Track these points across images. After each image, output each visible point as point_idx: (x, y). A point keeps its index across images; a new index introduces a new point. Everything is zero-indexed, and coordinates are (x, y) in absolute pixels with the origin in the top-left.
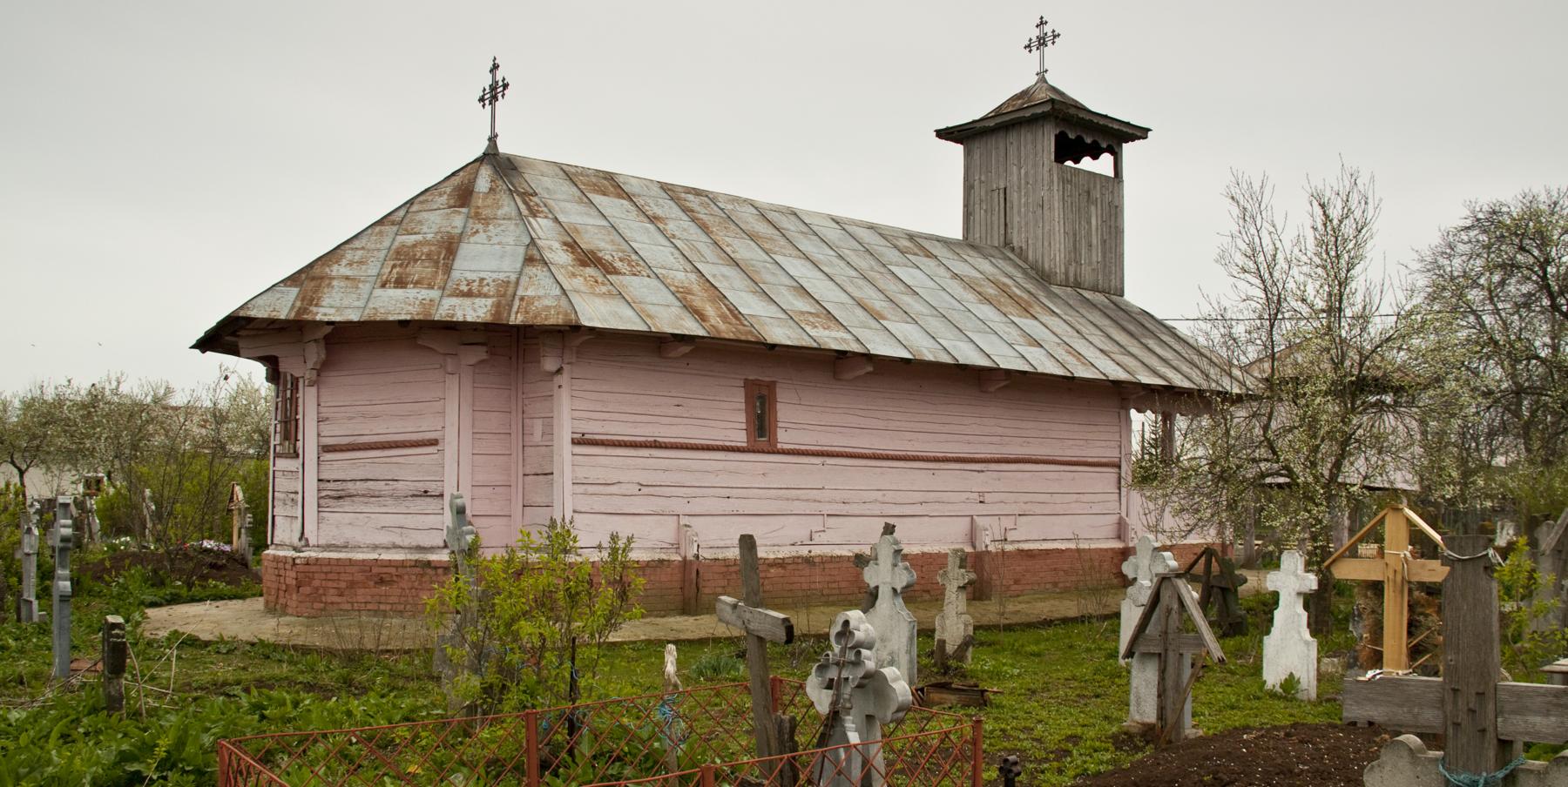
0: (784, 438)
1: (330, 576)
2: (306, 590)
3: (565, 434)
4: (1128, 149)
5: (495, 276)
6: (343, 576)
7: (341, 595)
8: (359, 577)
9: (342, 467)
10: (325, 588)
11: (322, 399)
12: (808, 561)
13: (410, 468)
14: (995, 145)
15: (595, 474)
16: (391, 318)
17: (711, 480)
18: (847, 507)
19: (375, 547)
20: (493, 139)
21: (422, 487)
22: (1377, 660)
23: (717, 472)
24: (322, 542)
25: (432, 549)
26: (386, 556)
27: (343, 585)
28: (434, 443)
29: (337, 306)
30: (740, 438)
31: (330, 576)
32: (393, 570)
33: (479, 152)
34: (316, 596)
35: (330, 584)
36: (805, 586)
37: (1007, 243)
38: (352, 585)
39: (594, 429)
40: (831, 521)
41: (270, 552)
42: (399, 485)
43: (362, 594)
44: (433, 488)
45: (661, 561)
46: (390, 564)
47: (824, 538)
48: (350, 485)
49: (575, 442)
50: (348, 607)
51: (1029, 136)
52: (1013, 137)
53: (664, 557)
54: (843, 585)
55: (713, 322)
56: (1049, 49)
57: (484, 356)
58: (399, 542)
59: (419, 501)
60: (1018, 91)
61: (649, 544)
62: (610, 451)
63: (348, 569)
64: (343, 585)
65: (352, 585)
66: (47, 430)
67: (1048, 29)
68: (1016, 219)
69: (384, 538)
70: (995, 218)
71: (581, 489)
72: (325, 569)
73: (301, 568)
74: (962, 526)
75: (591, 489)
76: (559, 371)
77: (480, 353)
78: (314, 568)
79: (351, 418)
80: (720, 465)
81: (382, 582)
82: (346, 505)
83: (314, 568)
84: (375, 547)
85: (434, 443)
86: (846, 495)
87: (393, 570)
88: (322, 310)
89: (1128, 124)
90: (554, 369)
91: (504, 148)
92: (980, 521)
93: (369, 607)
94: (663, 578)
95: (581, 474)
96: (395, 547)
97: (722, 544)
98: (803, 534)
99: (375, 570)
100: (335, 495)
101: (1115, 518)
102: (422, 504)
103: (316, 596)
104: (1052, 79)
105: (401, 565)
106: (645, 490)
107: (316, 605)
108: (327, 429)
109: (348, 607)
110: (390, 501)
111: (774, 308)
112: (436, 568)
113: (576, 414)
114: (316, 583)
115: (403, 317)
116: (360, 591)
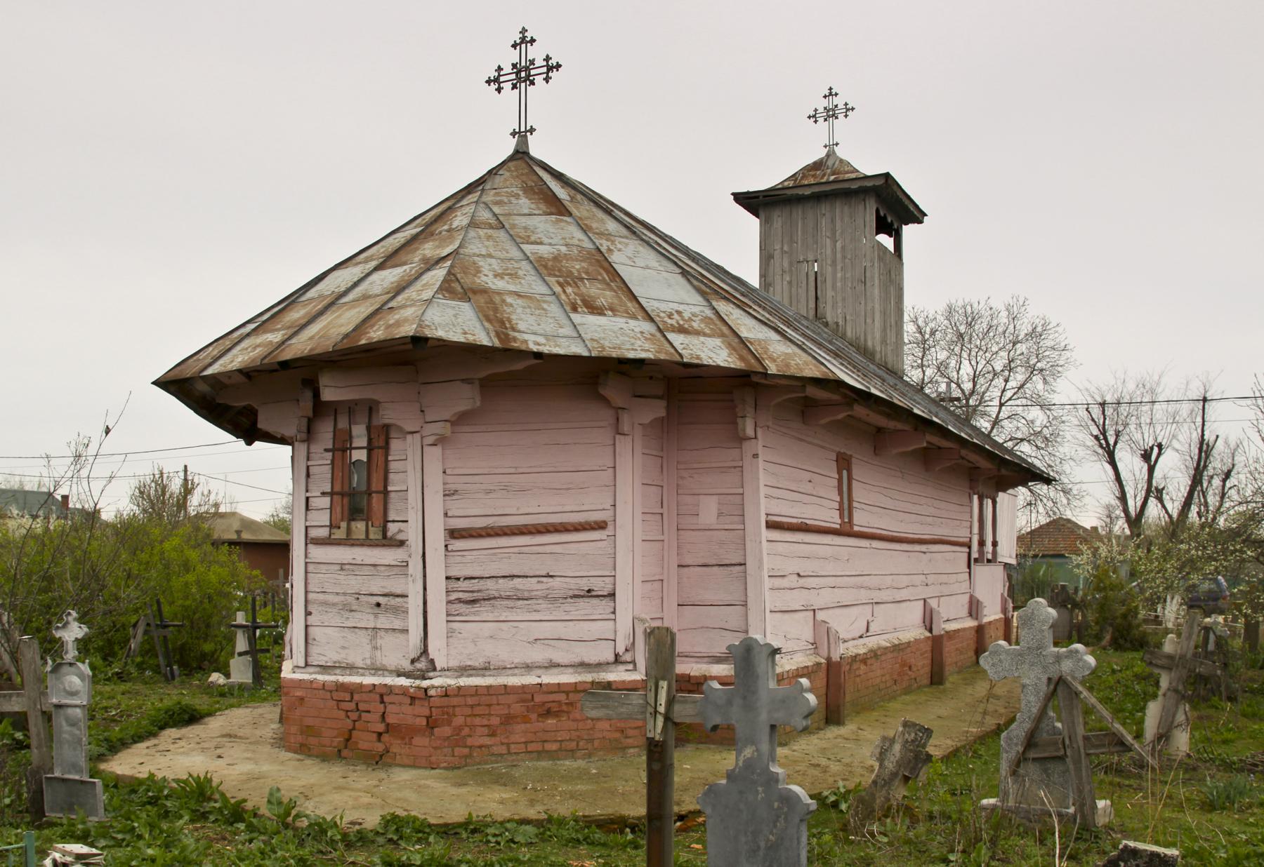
1: (478, 710)
2: (445, 731)
4: (908, 231)
6: (496, 710)
7: (493, 734)
8: (517, 709)
9: (479, 558)
10: (472, 727)
13: (572, 559)
14: (801, 217)
19: (528, 667)
20: (522, 135)
21: (585, 584)
25: (599, 666)
26: (550, 678)
27: (495, 721)
28: (601, 526)
31: (478, 710)
32: (562, 697)
33: (510, 151)
34: (457, 740)
35: (477, 721)
37: (818, 316)
38: (508, 720)
43: (519, 733)
46: (559, 688)
48: (490, 584)
49: (771, 525)
50: (503, 750)
51: (846, 209)
52: (825, 208)
56: (840, 122)
58: (559, 657)
59: (582, 603)
60: (810, 161)
63: (502, 699)
64: (495, 721)
65: (508, 720)
66: (20, 497)
67: (839, 101)
68: (830, 293)
69: (538, 655)
70: (802, 292)
72: (470, 701)
73: (436, 702)
74: (917, 611)
78: (455, 701)
79: (489, 492)
81: (548, 713)
82: (484, 612)
83: (455, 701)
84: (528, 667)
85: (601, 526)
87: (562, 697)
89: (601, 197)
91: (537, 149)
92: (933, 603)
93: (531, 747)
96: (552, 665)
99: (538, 699)
100: (469, 598)
101: (967, 597)
102: (585, 607)
103: (457, 740)
104: (840, 152)
105: (575, 688)
107: (458, 751)
108: (456, 507)
109: (503, 750)
110: (544, 605)
114: (459, 721)
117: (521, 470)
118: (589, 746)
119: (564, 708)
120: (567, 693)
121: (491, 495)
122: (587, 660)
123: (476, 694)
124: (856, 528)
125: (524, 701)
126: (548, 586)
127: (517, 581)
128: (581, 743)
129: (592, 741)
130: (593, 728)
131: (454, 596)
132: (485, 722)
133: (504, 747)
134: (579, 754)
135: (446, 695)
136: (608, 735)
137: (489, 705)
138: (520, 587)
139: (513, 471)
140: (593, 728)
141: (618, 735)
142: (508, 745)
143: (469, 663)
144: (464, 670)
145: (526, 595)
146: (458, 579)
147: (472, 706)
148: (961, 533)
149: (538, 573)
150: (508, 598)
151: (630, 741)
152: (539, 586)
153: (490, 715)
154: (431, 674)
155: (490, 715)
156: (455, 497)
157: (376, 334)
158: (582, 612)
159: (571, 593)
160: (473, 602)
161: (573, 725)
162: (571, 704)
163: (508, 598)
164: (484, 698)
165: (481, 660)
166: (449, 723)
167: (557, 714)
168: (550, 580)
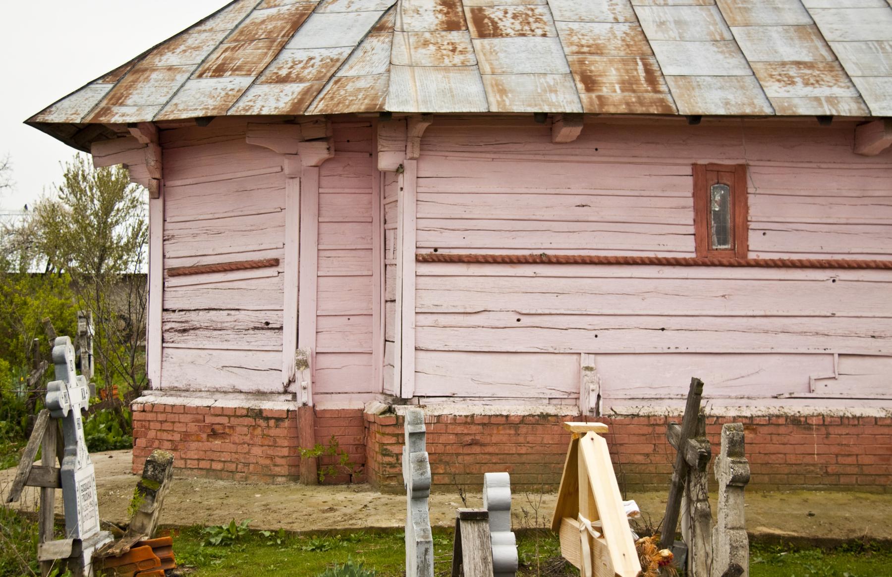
0: (758, 245)
1: (166, 426)
3: (405, 252)
5: (326, 53)
8: (193, 428)
10: (161, 440)
11: (169, 214)
12: (797, 422)
13: (250, 294)
15: (449, 301)
16: (184, 116)
17: (637, 306)
18: (878, 343)
21: (263, 317)
22: (396, 535)
23: (642, 295)
24: (165, 385)
27: (177, 437)
28: (275, 263)
29: (141, 106)
30: (686, 247)
31: (166, 426)
32: (225, 420)
35: (165, 436)
36: (792, 459)
38: (186, 437)
39: (451, 241)
40: (848, 365)
41: (148, 398)
42: (241, 315)
43: (194, 450)
44: (272, 318)
45: (544, 417)
46: (222, 412)
47: (833, 388)
48: (193, 316)
49: (421, 260)
53: (551, 410)
54: (867, 460)
55: (605, 91)
57: (325, 155)
61: (533, 393)
62: (668, 271)
63: (183, 418)
64: (177, 437)
65: (186, 437)
69: (224, 381)
71: (430, 319)
72: (161, 417)
75: (443, 320)
76: (400, 169)
77: (316, 154)
78: (150, 416)
79: (195, 236)
80: (650, 285)
81: (214, 434)
82: (190, 340)
83: (150, 416)
85: (275, 263)
86: (876, 326)
87: (225, 420)
88: (123, 110)
90: (394, 167)
94: (547, 439)
95: (429, 301)
97: (652, 393)
98: (797, 383)
105: (234, 414)
106: (525, 320)
110: (232, 335)
111: (737, 60)
112: (267, 419)
113: (423, 224)
114: (152, 434)
115: (200, 114)
116: (194, 445)
117: (217, 216)
118: (246, 470)
119: (227, 430)
120: (229, 417)
121: (197, 239)
122: (262, 389)
123: (164, 412)
124: (752, 256)
125: (198, 421)
126: (235, 318)
127: (212, 313)
128: (239, 466)
129: (247, 465)
130: (248, 453)
131: (168, 326)
132: (170, 438)
133: (183, 462)
134: (238, 476)
135: (144, 411)
136: (262, 461)
137: (174, 422)
138: (214, 319)
139: (210, 216)
140: (248, 453)
141: (268, 462)
142: (185, 459)
143: (176, 385)
144: (174, 390)
145: (219, 326)
146: (174, 311)
147: (161, 422)
148: (170, 260)
149: (229, 307)
150: (207, 328)
151: (277, 469)
152: (229, 319)
153: (173, 431)
154: (145, 392)
155: (173, 431)
156: (173, 241)
157: (317, 108)
158: (259, 343)
159: (252, 325)
160: (185, 331)
161: (232, 447)
162: (232, 427)
163: (207, 328)
164: (170, 416)
165: (185, 382)
166: (145, 435)
167: (223, 436)
168: (237, 312)
